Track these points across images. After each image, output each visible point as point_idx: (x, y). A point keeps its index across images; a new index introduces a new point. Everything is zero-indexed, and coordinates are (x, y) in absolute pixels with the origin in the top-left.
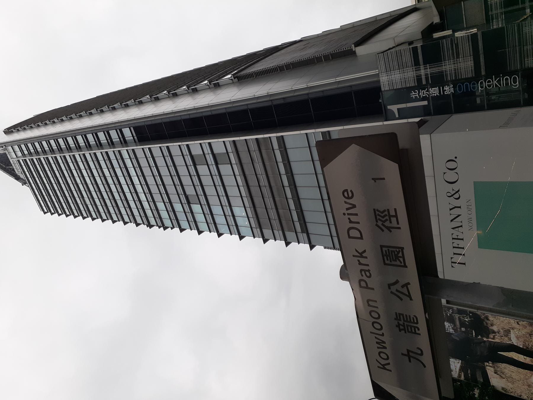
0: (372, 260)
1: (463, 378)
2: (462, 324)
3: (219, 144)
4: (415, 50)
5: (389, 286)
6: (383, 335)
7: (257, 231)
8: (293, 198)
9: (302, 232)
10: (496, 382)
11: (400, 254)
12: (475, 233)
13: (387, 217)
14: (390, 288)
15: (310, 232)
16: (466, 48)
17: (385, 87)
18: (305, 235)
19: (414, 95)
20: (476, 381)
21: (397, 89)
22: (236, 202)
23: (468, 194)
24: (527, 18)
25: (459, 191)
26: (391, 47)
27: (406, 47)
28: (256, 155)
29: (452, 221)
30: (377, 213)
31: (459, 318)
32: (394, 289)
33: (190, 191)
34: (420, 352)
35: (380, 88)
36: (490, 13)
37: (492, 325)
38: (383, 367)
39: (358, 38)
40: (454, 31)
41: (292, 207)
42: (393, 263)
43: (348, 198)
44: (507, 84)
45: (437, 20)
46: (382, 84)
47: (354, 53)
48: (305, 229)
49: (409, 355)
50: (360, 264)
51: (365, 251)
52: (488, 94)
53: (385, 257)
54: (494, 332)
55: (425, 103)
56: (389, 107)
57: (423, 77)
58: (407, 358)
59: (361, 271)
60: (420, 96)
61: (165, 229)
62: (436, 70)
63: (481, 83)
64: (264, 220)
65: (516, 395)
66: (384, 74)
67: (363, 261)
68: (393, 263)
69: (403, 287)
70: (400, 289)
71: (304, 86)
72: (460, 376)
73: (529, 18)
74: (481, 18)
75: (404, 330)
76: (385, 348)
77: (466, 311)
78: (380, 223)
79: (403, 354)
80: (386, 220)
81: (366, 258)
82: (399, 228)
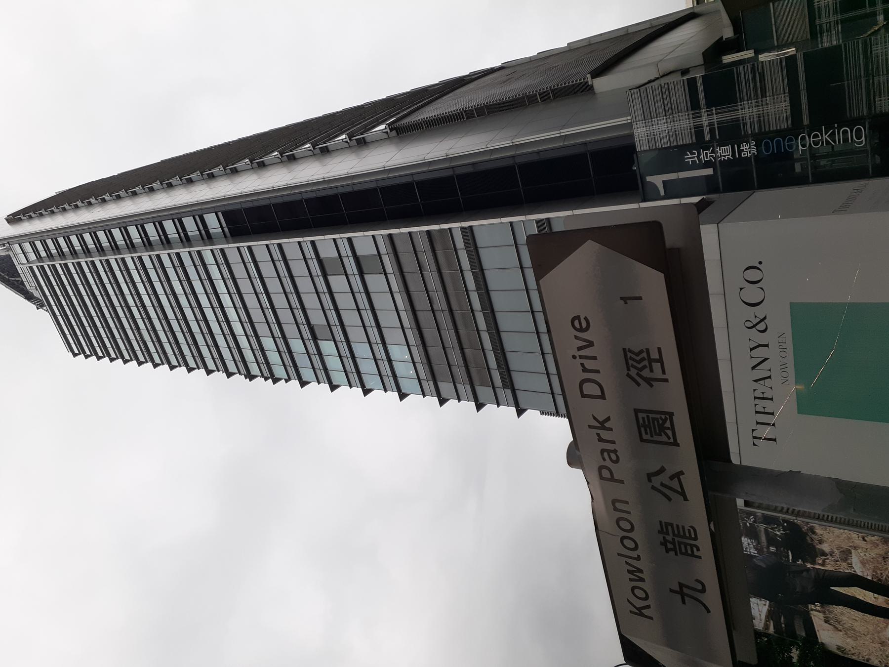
0: (621, 434)
1: (771, 630)
2: (771, 540)
3: (365, 240)
4: (692, 83)
5: (650, 476)
6: (638, 558)
7: (429, 385)
8: (488, 330)
9: (505, 387)
10: (827, 636)
11: (668, 424)
12: (793, 388)
13: (646, 363)
14: (650, 480)
15: (516, 387)
16: (778, 81)
17: (642, 145)
18: (509, 392)
19: (690, 158)
20: (794, 635)
21: (662, 148)
22: (394, 336)
23: (780, 323)
24: (879, 30)
25: (765, 318)
26: (653, 78)
27: (677, 78)
28: (426, 258)
29: (753, 368)
30: (629, 354)
31: (766, 530)
32: (656, 481)
33: (317, 318)
34: (700, 587)
35: (633, 147)
36: (817, 22)
37: (821, 542)
38: (639, 612)
39: (598, 64)
40: (757, 52)
41: (488, 345)
42: (656, 438)
43: (581, 330)
44: (846, 140)
45: (728, 33)
46: (637, 140)
47: (591, 88)
48: (509, 383)
49: (682, 591)
50: (600, 440)
51: (608, 419)
52: (814, 156)
53: (643, 429)
54: (824, 554)
55: (709, 171)
56: (649, 179)
57: (706, 129)
58: (679, 597)
59: (603, 451)
60: (700, 160)
61: (274, 382)
62: (727, 116)
63: (803, 138)
64: (440, 367)
65: (861, 659)
66: (641, 124)
67: (605, 435)
68: (656, 438)
69: (672, 478)
70: (667, 482)
71: (507, 143)
72: (767, 627)
73: (883, 31)
74: (802, 29)
75: (674, 550)
76: (642, 580)
77: (777, 519)
78: (633, 372)
79: (671, 591)
80: (645, 367)
81: (611, 429)
82: (666, 380)
